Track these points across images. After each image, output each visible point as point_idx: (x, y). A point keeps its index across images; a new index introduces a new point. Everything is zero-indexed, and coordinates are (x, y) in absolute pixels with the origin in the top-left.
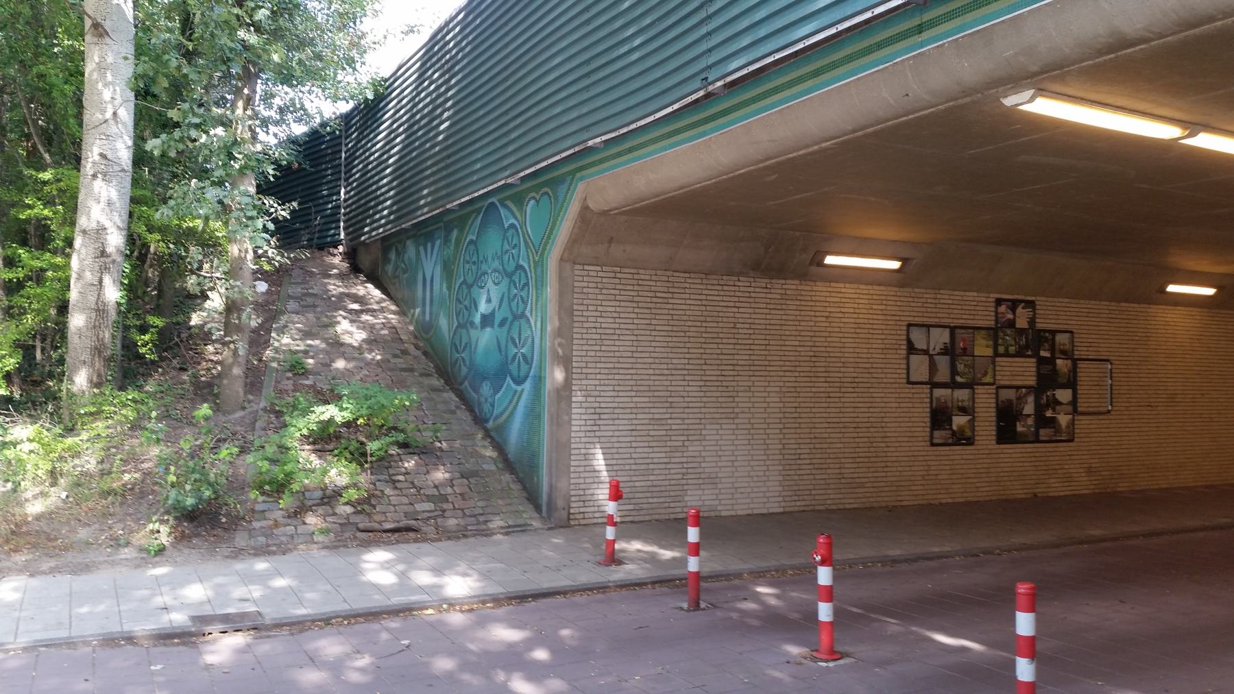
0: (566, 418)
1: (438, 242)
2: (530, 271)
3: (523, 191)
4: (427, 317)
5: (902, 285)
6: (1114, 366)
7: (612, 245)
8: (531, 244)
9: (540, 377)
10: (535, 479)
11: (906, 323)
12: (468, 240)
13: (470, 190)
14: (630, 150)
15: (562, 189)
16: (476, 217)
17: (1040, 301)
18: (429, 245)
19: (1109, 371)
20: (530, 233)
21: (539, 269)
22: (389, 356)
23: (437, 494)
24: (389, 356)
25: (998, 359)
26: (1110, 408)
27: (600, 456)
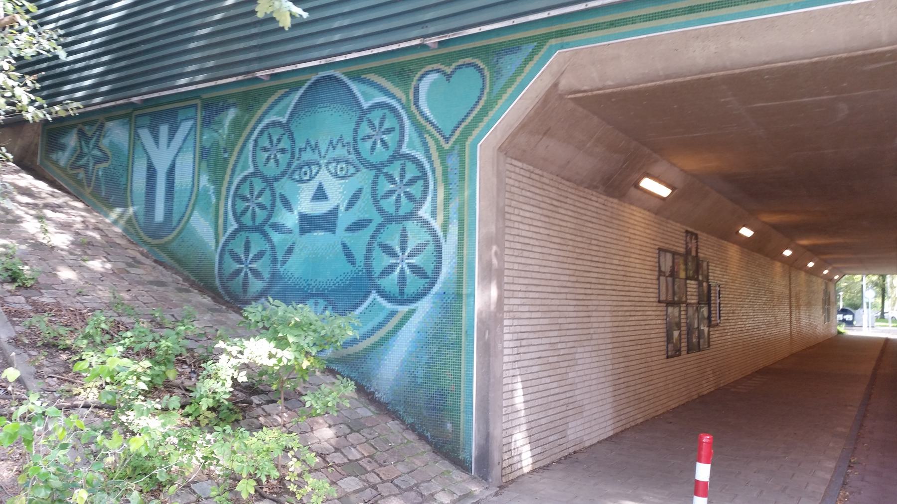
0: (500, 346)
1: (185, 127)
2: (431, 163)
3: (410, 62)
4: (159, 215)
5: (657, 212)
6: (722, 289)
7: (544, 138)
8: (429, 127)
9: (459, 296)
10: (449, 426)
11: (657, 247)
12: (266, 121)
13: (326, 52)
14: (613, 24)
15: (510, 63)
16: (286, 95)
17: (702, 236)
18: (164, 130)
19: (717, 292)
20: (432, 117)
21: (453, 161)
22: (123, 265)
23: (346, 461)
24: (123, 265)
25: (688, 281)
26: (719, 321)
27: (520, 393)
